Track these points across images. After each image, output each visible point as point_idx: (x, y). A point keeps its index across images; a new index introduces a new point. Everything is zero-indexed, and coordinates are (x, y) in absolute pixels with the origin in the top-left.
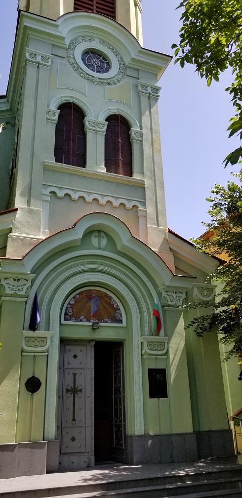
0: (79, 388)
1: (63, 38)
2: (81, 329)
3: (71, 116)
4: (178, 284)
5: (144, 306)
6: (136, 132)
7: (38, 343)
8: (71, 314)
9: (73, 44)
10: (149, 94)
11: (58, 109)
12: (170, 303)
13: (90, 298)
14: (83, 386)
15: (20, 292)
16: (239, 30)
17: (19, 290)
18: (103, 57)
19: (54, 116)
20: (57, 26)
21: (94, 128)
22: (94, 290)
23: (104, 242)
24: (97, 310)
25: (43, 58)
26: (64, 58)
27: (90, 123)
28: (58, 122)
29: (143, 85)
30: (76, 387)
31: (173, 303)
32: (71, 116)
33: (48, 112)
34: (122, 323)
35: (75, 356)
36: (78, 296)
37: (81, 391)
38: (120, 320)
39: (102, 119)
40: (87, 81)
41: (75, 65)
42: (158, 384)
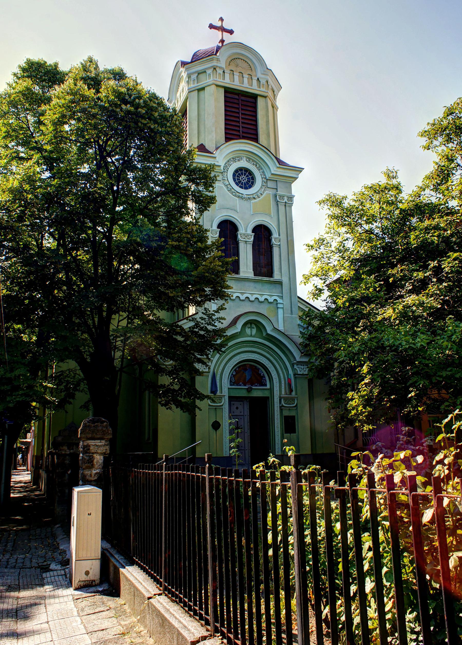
1: (220, 166)
2: (241, 391)
5: (281, 375)
10: (286, 203)
12: (299, 373)
13: (246, 370)
14: (243, 426)
16: (77, 115)
23: (254, 331)
31: (301, 373)
35: (237, 408)
39: (249, 231)
41: (229, 186)
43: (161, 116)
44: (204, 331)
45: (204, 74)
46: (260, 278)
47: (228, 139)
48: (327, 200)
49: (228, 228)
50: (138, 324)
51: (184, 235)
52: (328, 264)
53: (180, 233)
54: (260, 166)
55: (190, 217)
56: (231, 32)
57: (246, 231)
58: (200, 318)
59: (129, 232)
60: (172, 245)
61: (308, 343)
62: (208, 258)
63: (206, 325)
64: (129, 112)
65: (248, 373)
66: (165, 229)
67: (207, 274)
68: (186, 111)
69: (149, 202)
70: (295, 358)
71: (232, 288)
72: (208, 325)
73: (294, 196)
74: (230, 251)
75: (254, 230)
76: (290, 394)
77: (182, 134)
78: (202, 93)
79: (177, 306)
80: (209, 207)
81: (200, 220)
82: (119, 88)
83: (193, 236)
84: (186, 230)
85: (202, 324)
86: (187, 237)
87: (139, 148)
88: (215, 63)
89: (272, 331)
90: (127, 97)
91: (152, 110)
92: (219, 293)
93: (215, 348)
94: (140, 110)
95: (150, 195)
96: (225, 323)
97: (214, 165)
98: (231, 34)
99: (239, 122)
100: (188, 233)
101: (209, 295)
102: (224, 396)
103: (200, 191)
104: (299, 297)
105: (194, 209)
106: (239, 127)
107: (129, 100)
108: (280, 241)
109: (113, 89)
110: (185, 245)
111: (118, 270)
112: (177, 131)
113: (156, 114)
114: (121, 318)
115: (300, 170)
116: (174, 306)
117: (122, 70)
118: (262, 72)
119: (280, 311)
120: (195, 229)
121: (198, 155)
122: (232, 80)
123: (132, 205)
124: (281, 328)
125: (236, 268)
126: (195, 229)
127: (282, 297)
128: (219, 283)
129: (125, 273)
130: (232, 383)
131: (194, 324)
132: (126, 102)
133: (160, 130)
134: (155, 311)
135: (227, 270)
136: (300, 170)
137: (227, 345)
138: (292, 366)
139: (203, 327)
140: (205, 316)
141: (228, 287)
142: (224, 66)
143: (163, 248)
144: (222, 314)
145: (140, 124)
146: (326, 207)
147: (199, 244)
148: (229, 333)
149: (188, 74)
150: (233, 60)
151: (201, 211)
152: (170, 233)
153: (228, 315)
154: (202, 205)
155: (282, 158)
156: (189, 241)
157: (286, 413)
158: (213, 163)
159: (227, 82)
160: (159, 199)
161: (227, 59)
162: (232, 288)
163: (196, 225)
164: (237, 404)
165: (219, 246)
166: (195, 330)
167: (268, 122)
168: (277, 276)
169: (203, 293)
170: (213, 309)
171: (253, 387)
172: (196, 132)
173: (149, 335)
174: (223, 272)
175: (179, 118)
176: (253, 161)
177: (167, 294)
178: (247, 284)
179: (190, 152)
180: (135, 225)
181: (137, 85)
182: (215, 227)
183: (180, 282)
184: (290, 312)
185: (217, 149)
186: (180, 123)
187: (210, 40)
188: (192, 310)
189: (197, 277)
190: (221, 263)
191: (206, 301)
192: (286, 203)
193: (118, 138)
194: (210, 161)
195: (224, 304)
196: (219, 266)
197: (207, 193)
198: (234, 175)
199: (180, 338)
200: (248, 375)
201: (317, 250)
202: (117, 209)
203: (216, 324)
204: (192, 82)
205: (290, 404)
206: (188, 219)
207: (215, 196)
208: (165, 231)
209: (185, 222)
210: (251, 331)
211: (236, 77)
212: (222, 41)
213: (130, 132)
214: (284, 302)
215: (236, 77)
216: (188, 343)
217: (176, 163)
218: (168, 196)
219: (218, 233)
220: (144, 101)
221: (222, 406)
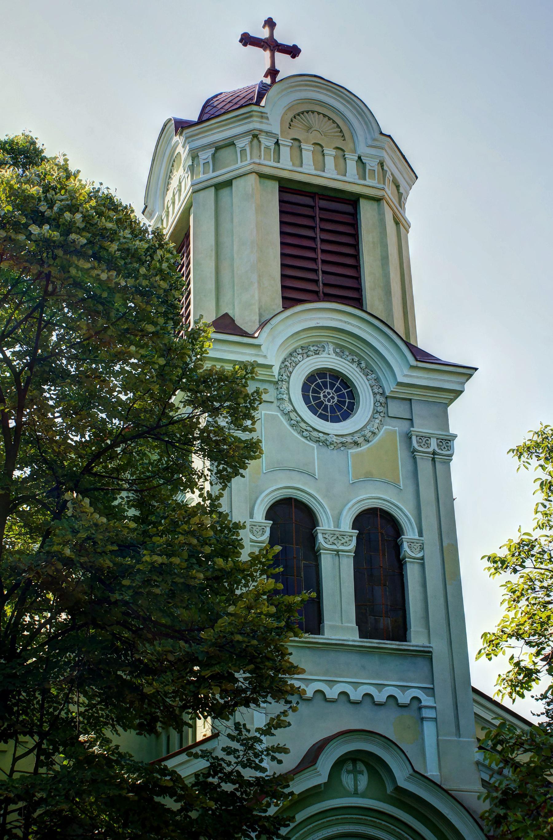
1: (270, 367)
6: (411, 542)
10: (434, 453)
11: (267, 518)
18: (342, 380)
19: (263, 534)
21: (334, 547)
23: (363, 781)
26: (272, 402)
27: (326, 536)
29: (420, 437)
39: (346, 525)
41: (293, 415)
43: (126, 251)
44: (234, 783)
45: (230, 150)
47: (289, 302)
48: (538, 445)
49: (293, 518)
50: (63, 767)
51: (181, 538)
52: (545, 605)
53: (174, 532)
54: (368, 365)
55: (197, 492)
56: (293, 51)
57: (337, 525)
58: (223, 749)
59: (46, 534)
60: (152, 564)
61: (502, 812)
62: (241, 595)
63: (239, 768)
64: (46, 243)
66: (133, 525)
67: (239, 638)
68: (187, 236)
69: (96, 457)
71: (303, 671)
72: (244, 766)
73: (456, 436)
74: (299, 575)
77: (177, 294)
78: (224, 192)
79: (162, 718)
80: (245, 468)
81: (222, 501)
82: (25, 186)
83: (205, 542)
84: (186, 527)
85: (229, 764)
86: (190, 544)
87: (71, 327)
88: (255, 124)
89: (408, 779)
90: (43, 207)
91: (103, 236)
92: (271, 681)
93: (263, 827)
94: (73, 236)
95: (98, 438)
96: (290, 762)
97: (255, 365)
98: (293, 57)
99: (314, 250)
100: (192, 533)
101: (244, 691)
103: (221, 429)
104: (475, 691)
105: (206, 472)
106: (315, 271)
107: (48, 213)
108: (422, 549)
109: (11, 187)
110: (185, 565)
111: (16, 625)
112: (164, 285)
113: (114, 247)
114: (21, 751)
115: (468, 372)
116: (155, 719)
117: (33, 143)
118: (370, 142)
119: (429, 729)
120: (208, 523)
121: (217, 340)
122: (298, 162)
123: (51, 465)
124: (432, 772)
125: (313, 620)
126: (208, 523)
127: (431, 691)
128: (268, 659)
129: (35, 634)
131: (208, 764)
132: (40, 219)
133: (123, 283)
134: (108, 732)
135: (289, 627)
136: (468, 372)
137: (292, 819)
139: (231, 773)
140: (235, 745)
141: (293, 670)
142: (276, 130)
143: (127, 571)
144: (280, 737)
145: (73, 271)
146: (534, 462)
147: (220, 561)
148: (298, 787)
149: (191, 150)
150: (299, 115)
151: (224, 479)
152: (145, 533)
153: (297, 738)
154: (226, 463)
155: (422, 344)
156: (193, 554)
158: (251, 359)
159: (286, 166)
160: (119, 450)
161: (285, 113)
162: (303, 671)
163: (211, 512)
165: (269, 567)
166: (210, 780)
167: (385, 259)
168: (417, 639)
169: (229, 686)
170: (257, 725)
172: (211, 285)
173: (90, 794)
174: (279, 631)
175: (168, 255)
176: (352, 353)
177: (137, 689)
178: (343, 658)
179: (194, 336)
180: (58, 515)
181: (68, 177)
182: (260, 515)
183: (171, 658)
184: (454, 729)
185: (263, 325)
186: (173, 267)
187: (246, 71)
188: (203, 728)
189: (214, 644)
190: (273, 609)
191: (236, 705)
192: (434, 453)
193: (21, 303)
194: (245, 356)
195: (284, 713)
196: (269, 615)
197: (239, 434)
198: (305, 389)
199: (171, 804)
201: (515, 571)
202: (17, 473)
203: (264, 765)
204: (201, 168)
206: (192, 498)
207: (259, 441)
208: (135, 529)
209: (183, 506)
210: (356, 780)
211: (307, 156)
212: (273, 72)
213: (50, 288)
214: (437, 704)
215: (307, 156)
216: (194, 815)
217: (162, 361)
218: (141, 441)
219: (268, 530)
220: (84, 217)
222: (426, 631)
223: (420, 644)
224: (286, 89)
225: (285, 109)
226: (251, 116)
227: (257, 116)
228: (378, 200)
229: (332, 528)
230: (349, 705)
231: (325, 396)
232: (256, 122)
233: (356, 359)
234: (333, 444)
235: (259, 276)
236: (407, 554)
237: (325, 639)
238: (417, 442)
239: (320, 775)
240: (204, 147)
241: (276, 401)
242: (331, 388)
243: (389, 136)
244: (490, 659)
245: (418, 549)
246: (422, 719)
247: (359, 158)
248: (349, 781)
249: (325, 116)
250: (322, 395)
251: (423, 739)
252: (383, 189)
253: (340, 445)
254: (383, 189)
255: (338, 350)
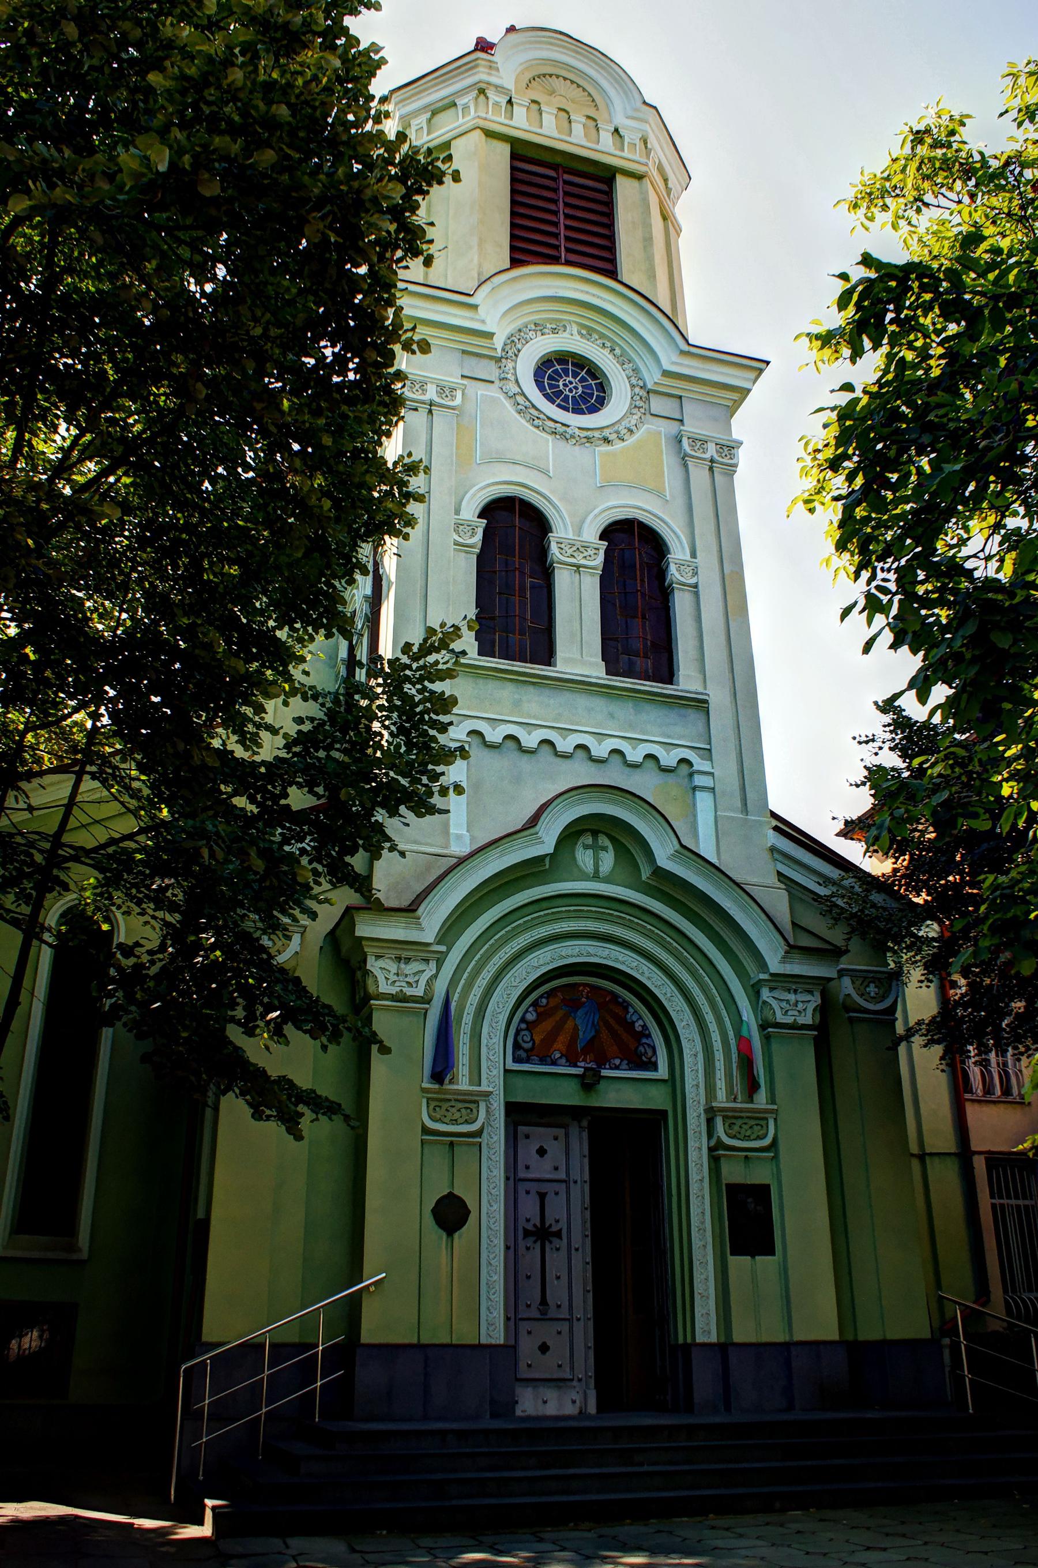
0: (554, 1229)
1: (490, 335)
3: (514, 531)
4: (798, 968)
5: (713, 1027)
6: (680, 566)
7: (457, 1115)
8: (530, 1045)
9: (515, 342)
10: (712, 461)
12: (780, 1018)
13: (574, 1005)
14: (563, 1225)
15: (411, 989)
17: (409, 984)
18: (589, 370)
19: (472, 536)
20: (474, 307)
22: (585, 985)
23: (608, 860)
24: (594, 1037)
25: (441, 389)
27: (562, 546)
28: (482, 549)
30: (547, 1225)
31: (789, 1020)
32: (514, 531)
33: (458, 525)
34: (656, 1069)
35: (542, 1152)
36: (544, 1001)
37: (558, 1234)
38: (650, 1062)
39: (591, 533)
40: (550, 438)
41: (520, 399)
42: (749, 1224)
46: (627, 683)
54: (624, 353)
57: (579, 531)
65: (587, 1017)
70: (763, 965)
75: (608, 533)
76: (750, 1099)
102: (487, 1094)
108: (695, 573)
118: (630, 113)
119: (704, 802)
127: (707, 753)
130: (521, 1052)
136: (758, 366)
138: (754, 991)
157: (734, 1173)
159: (521, 123)
161: (522, 72)
164: (541, 1135)
168: (687, 681)
171: (605, 1073)
176: (602, 336)
192: (712, 461)
200: (582, 1025)
205: (747, 1138)
221: (479, 1133)
222: (702, 676)
223: (693, 688)
224: (523, 43)
225: (522, 67)
226: (476, 66)
227: (485, 66)
228: (639, 177)
229: (571, 536)
230: (590, 763)
231: (565, 385)
232: (483, 72)
233: (608, 344)
234: (574, 437)
235: (480, 239)
236: (674, 579)
237: (557, 672)
238: (689, 445)
239: (543, 842)
240: (416, 113)
241: (497, 381)
242: (574, 377)
243: (655, 108)
244: (811, 511)
245: (690, 574)
246: (695, 789)
247: (616, 130)
248: (587, 860)
249: (572, 82)
250: (561, 383)
251: (695, 816)
252: (646, 165)
253: (585, 440)
254: (646, 165)
255: (584, 332)
